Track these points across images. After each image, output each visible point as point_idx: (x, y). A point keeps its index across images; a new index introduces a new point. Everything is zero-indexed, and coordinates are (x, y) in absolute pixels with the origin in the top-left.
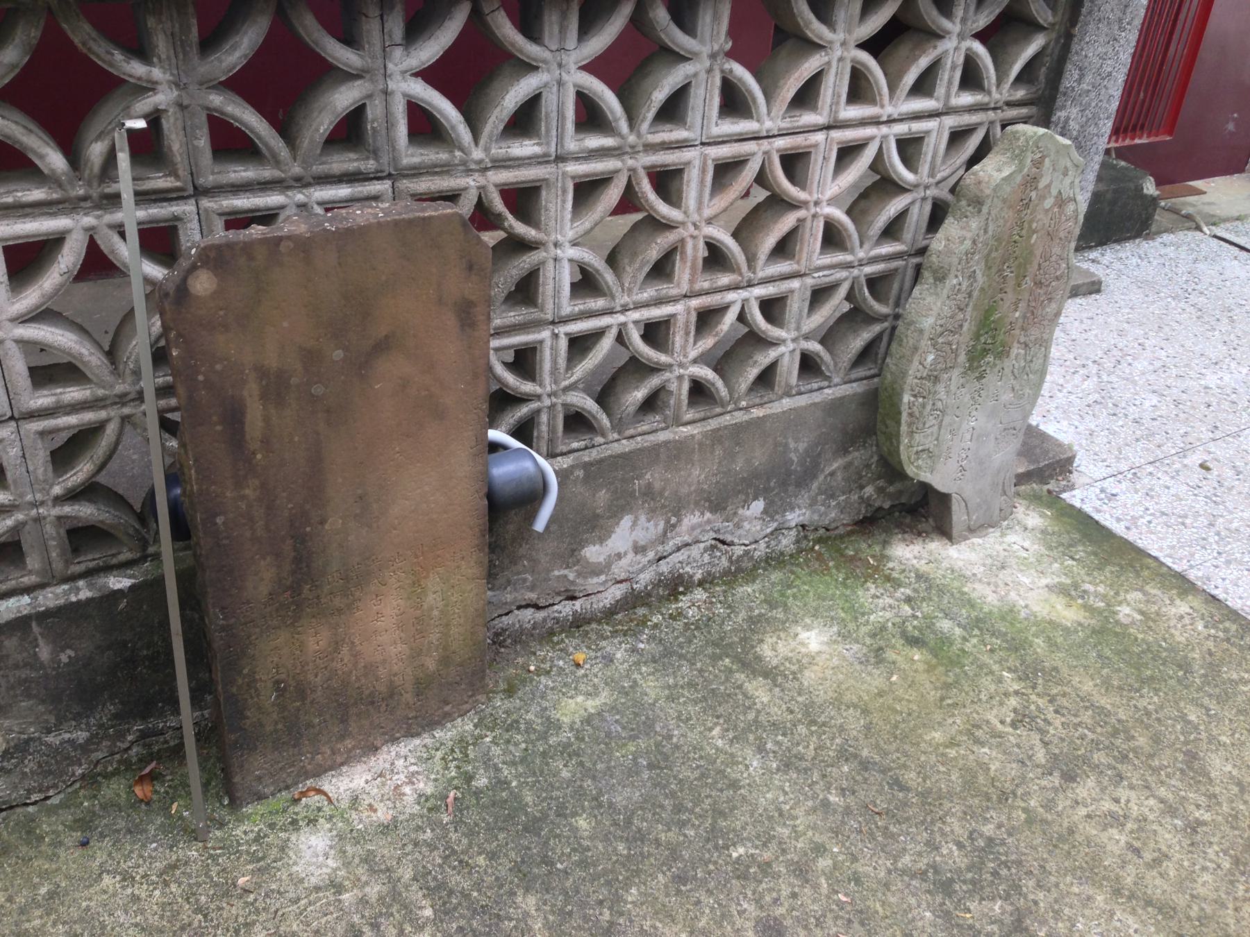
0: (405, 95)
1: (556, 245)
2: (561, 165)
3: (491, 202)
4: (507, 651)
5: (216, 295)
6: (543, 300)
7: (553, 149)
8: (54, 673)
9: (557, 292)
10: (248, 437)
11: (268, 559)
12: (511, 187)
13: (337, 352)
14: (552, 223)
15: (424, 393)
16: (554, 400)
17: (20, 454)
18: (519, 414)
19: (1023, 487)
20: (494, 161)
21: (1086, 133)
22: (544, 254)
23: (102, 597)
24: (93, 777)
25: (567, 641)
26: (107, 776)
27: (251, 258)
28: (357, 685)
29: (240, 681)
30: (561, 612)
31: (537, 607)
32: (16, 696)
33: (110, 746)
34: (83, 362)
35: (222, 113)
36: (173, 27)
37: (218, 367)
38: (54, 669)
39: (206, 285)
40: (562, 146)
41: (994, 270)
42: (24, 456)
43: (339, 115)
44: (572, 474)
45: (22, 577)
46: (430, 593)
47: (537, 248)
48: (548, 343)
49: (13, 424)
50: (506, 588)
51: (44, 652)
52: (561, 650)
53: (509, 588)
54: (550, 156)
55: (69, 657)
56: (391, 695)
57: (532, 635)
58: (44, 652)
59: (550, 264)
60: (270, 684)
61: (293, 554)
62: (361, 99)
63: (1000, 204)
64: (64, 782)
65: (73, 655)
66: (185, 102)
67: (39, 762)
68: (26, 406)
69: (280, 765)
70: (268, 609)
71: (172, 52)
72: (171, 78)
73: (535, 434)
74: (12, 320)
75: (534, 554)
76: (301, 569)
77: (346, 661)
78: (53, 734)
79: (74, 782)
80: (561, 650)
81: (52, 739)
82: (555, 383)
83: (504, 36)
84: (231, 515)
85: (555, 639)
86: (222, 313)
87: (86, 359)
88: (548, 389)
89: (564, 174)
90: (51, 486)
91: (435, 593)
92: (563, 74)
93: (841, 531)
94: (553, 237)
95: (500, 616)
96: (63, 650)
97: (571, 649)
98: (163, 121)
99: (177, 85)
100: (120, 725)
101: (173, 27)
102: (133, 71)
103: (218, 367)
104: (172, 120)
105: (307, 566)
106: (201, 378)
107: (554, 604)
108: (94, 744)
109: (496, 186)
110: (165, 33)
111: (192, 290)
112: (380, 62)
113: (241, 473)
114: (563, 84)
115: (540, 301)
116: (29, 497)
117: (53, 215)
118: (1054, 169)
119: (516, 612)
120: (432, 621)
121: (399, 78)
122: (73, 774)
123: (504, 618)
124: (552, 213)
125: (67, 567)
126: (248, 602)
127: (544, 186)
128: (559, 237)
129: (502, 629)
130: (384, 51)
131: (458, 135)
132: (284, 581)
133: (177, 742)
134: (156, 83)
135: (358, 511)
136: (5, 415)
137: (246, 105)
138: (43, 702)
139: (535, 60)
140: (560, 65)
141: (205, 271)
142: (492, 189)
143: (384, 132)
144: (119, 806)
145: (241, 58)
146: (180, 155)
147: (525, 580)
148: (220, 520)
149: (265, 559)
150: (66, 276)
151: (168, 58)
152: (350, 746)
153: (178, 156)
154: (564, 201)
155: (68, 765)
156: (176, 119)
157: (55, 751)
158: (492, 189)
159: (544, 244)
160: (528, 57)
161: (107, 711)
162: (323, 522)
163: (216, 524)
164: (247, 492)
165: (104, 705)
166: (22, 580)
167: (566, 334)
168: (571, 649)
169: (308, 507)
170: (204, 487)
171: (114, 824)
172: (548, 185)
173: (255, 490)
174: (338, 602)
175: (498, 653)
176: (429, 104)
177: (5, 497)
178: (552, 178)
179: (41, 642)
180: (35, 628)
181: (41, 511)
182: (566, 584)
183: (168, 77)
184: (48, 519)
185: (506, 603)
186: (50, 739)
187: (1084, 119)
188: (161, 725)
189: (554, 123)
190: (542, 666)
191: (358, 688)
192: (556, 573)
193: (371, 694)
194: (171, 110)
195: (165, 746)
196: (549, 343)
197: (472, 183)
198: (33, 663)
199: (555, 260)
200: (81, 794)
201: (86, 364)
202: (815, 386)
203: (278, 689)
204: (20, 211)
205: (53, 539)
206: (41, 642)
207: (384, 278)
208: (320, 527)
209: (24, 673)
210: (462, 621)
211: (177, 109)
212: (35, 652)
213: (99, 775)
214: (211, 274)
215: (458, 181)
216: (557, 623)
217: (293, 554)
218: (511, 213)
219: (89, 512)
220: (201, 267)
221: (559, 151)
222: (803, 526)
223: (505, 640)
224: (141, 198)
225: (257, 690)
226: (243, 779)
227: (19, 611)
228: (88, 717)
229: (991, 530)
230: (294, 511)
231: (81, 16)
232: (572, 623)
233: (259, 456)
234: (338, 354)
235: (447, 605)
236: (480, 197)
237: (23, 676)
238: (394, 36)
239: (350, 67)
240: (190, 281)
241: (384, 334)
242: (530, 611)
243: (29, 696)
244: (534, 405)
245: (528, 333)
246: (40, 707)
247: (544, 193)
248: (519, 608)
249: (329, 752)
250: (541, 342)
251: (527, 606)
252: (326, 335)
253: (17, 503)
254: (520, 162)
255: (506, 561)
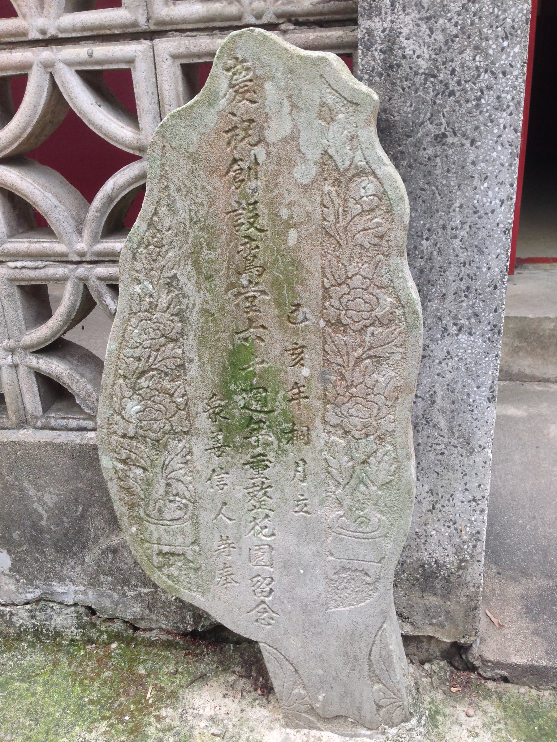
19: (523, 690)
21: (456, 64)
41: (220, 283)
63: (186, 166)
93: (153, 635)
118: (294, 106)
137: (53, 171)
187: (440, 37)
202: (73, 423)
222: (92, 611)
224: (115, 259)
229: (364, 731)
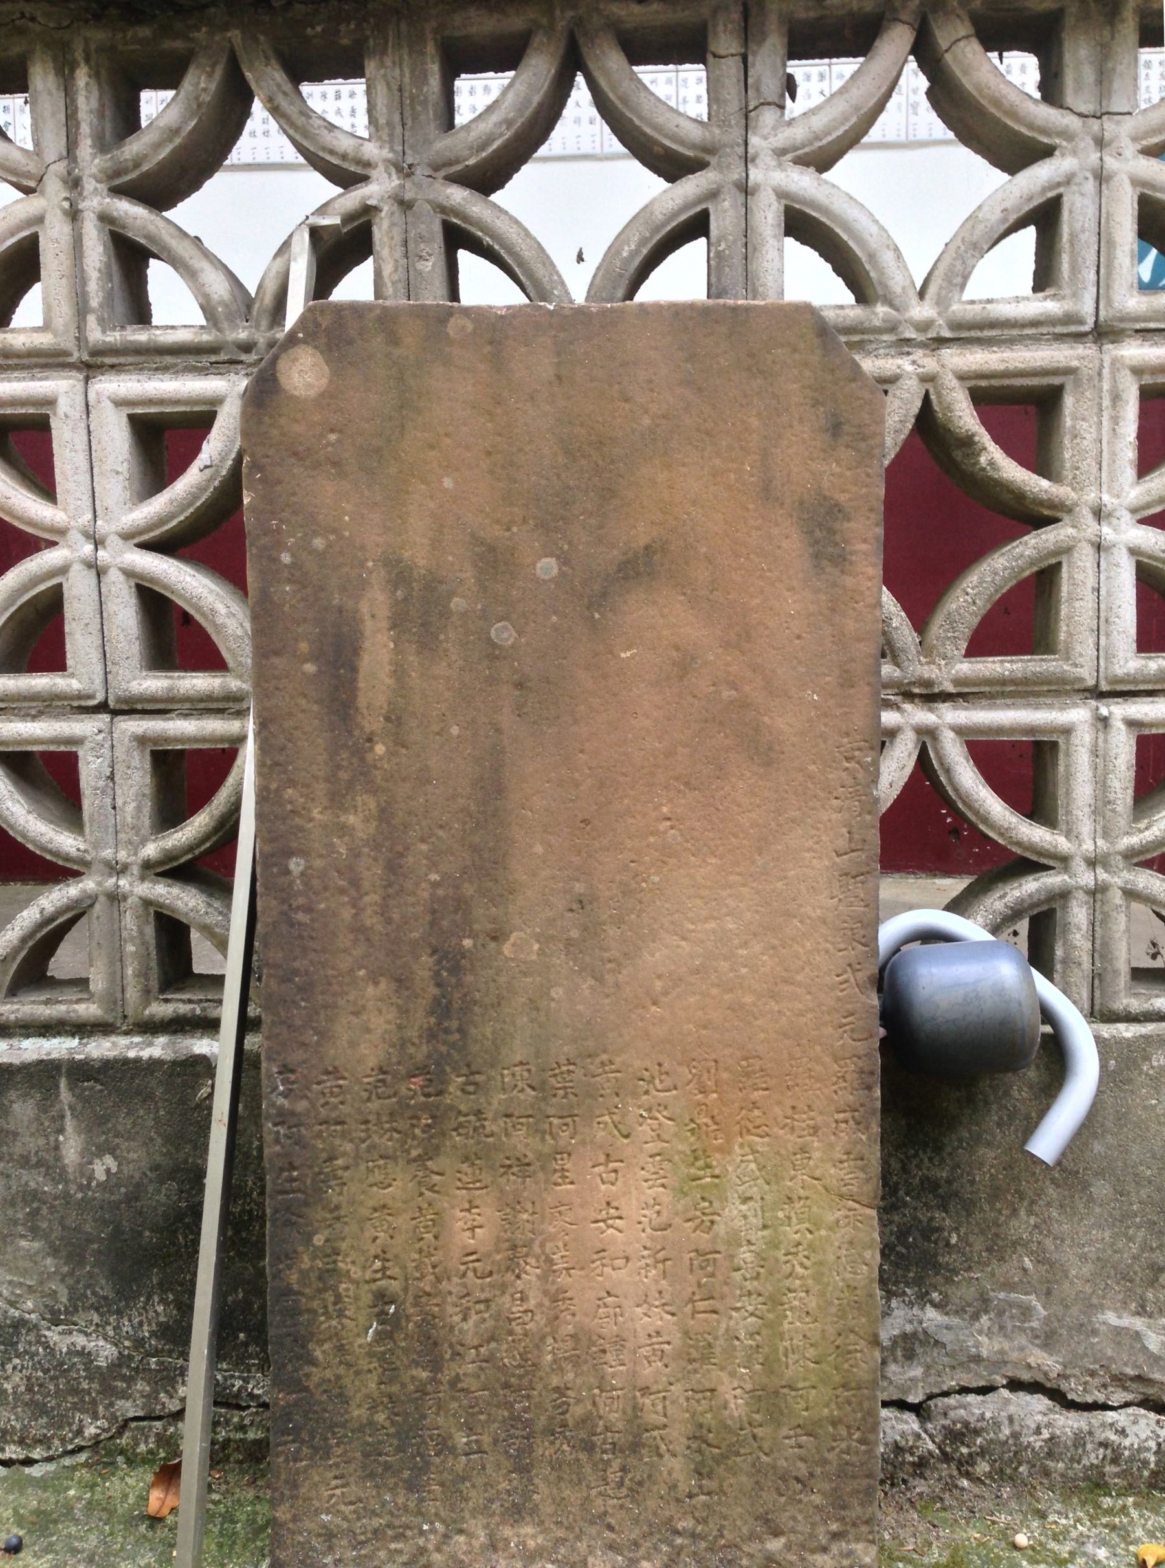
0: (781, 194)
1: (1099, 513)
2: (1108, 347)
3: (949, 408)
4: (976, 1490)
5: (326, 397)
6: (1070, 634)
7: (1087, 307)
8: (80, 1195)
9: (1101, 625)
10: (362, 702)
11: (383, 984)
12: (995, 382)
13: (546, 561)
14: (1088, 465)
15: (727, 694)
16: (1102, 875)
17: (108, 772)
18: (1017, 893)
20: (956, 326)
22: (1070, 531)
23: (174, 1063)
24: (109, 1453)
25: (1135, 1514)
26: (132, 1461)
27: (394, 340)
28: (555, 1381)
29: (306, 1262)
30: (1123, 1432)
31: (1058, 1396)
32: (15, 1222)
33: (148, 1396)
34: (215, 625)
35: (466, 218)
36: (402, 75)
37: (319, 543)
38: (81, 1188)
39: (310, 378)
40: (1109, 303)
42: (111, 777)
43: (657, 229)
44: (1147, 1058)
45: (78, 1001)
46: (733, 1197)
47: (1055, 520)
48: (1084, 738)
49: (106, 717)
50: (976, 1317)
51: (72, 1148)
52: (1113, 1528)
53: (984, 1319)
54: (1081, 322)
55: (108, 1171)
56: (635, 1446)
57: (1047, 1473)
58: (72, 1148)
59: (1084, 557)
60: (367, 1298)
61: (434, 991)
62: (700, 200)
64: (63, 1440)
65: (114, 1170)
66: (408, 196)
67: (29, 1378)
68: (124, 686)
69: (376, 1522)
70: (375, 1105)
71: (397, 118)
72: (390, 156)
73: (1059, 952)
74: (126, 536)
75: (1049, 1243)
76: (447, 1031)
77: (532, 1303)
78: (60, 1328)
79: (80, 1449)
80: (1113, 1528)
81: (56, 1338)
82: (1106, 835)
83: (978, 87)
84: (318, 863)
85: (1107, 1502)
86: (333, 437)
87: (220, 620)
88: (1088, 846)
89: (1114, 361)
90: (143, 842)
91: (746, 1200)
92: (1107, 159)
94: (1091, 496)
95: (964, 1390)
96: (101, 1151)
97: (1139, 1532)
98: (375, 229)
99: (399, 169)
100: (170, 1353)
101: (402, 75)
102: (335, 142)
103: (319, 543)
104: (385, 224)
105: (460, 1030)
106: (286, 558)
107: (1105, 1407)
108: (124, 1378)
109: (962, 377)
110: (388, 84)
111: (283, 380)
112: (736, 134)
113: (344, 775)
114: (1109, 178)
115: (1062, 636)
116: (108, 853)
117: (203, 371)
119: (1005, 1393)
120: (737, 1276)
121: (771, 161)
122: (79, 1432)
123: (971, 1398)
124: (1087, 443)
125: (147, 1003)
126: (334, 1073)
127: (1068, 388)
128: (1106, 498)
129: (966, 1424)
130: (747, 118)
131: (881, 272)
132: (412, 1050)
133: (260, 1435)
134: (368, 164)
135: (575, 934)
136: (90, 697)
138: (54, 1251)
139: (1044, 131)
140: (1100, 143)
141: (310, 350)
142: (950, 381)
143: (737, 260)
144: (111, 1512)
145: (500, 123)
146: (393, 283)
147: (1026, 1312)
148: (296, 865)
149: (376, 983)
150: (207, 471)
151: (389, 124)
152: (531, 1544)
153: (389, 284)
154: (1115, 420)
155: (75, 1407)
156: (393, 224)
157: (59, 1367)
158: (950, 381)
159: (1070, 511)
160: (1031, 126)
161: (151, 1314)
162: (497, 937)
163: (288, 872)
164: (351, 819)
165: (149, 1298)
166: (76, 1007)
167: (1131, 723)
168: (1139, 1532)
169: (469, 890)
170: (274, 786)
171: (81, 1539)
172: (1078, 383)
173: (367, 820)
174: (521, 1141)
175: (951, 1486)
176: (826, 211)
177: (75, 843)
178: (1087, 369)
179: (69, 1123)
180: (65, 1095)
181: (121, 883)
182: (1141, 1358)
183: (386, 153)
184: (130, 900)
185: (977, 1359)
186: (53, 1335)
188: (238, 1383)
189: (1091, 257)
190: (1052, 1545)
191: (557, 1389)
192: (1111, 1318)
193: (585, 1421)
194: (386, 208)
195: (239, 1436)
196: (1088, 738)
197: (909, 368)
198: (50, 1164)
199: (1098, 547)
200: (78, 1474)
201: (219, 628)
203: (382, 1317)
204: (158, 359)
205: (132, 939)
206: (69, 1123)
207: (647, 421)
208: (493, 945)
209: (35, 1180)
210: (813, 1303)
211: (395, 208)
212: (57, 1140)
213: (122, 1452)
214: (319, 358)
215: (880, 363)
216: (1115, 1461)
217: (434, 991)
218: (996, 440)
219: (192, 903)
220: (304, 341)
221: (1102, 313)
223: (971, 1460)
225: (338, 1299)
226: (295, 1519)
227: (49, 1054)
228: (119, 1313)
230: (440, 892)
231: (273, 62)
232: (1154, 1474)
233: (380, 749)
234: (548, 567)
235: (774, 1244)
236: (926, 399)
237: (32, 1185)
238: (763, 88)
239: (682, 142)
240: (282, 365)
241: (643, 541)
242: (1039, 1403)
243: (35, 1232)
244: (1052, 880)
245: (1037, 707)
246: (49, 1261)
247: (1069, 401)
248: (1015, 1385)
249: (482, 1537)
250: (1067, 731)
251: (1034, 1387)
252: (524, 521)
253: (89, 858)
254: (1015, 332)
255: (979, 1244)
